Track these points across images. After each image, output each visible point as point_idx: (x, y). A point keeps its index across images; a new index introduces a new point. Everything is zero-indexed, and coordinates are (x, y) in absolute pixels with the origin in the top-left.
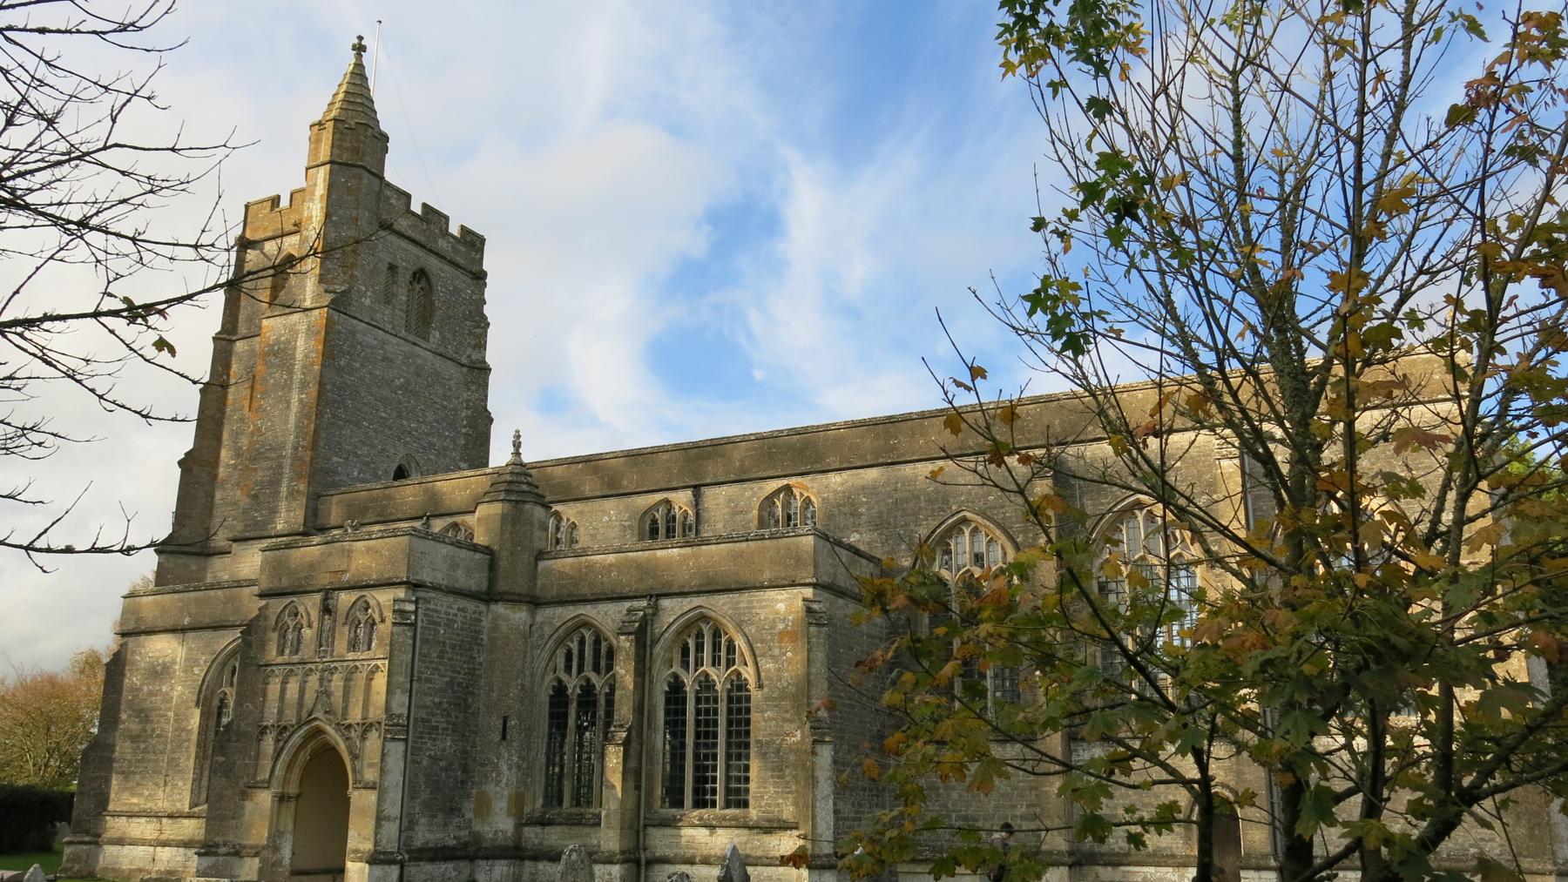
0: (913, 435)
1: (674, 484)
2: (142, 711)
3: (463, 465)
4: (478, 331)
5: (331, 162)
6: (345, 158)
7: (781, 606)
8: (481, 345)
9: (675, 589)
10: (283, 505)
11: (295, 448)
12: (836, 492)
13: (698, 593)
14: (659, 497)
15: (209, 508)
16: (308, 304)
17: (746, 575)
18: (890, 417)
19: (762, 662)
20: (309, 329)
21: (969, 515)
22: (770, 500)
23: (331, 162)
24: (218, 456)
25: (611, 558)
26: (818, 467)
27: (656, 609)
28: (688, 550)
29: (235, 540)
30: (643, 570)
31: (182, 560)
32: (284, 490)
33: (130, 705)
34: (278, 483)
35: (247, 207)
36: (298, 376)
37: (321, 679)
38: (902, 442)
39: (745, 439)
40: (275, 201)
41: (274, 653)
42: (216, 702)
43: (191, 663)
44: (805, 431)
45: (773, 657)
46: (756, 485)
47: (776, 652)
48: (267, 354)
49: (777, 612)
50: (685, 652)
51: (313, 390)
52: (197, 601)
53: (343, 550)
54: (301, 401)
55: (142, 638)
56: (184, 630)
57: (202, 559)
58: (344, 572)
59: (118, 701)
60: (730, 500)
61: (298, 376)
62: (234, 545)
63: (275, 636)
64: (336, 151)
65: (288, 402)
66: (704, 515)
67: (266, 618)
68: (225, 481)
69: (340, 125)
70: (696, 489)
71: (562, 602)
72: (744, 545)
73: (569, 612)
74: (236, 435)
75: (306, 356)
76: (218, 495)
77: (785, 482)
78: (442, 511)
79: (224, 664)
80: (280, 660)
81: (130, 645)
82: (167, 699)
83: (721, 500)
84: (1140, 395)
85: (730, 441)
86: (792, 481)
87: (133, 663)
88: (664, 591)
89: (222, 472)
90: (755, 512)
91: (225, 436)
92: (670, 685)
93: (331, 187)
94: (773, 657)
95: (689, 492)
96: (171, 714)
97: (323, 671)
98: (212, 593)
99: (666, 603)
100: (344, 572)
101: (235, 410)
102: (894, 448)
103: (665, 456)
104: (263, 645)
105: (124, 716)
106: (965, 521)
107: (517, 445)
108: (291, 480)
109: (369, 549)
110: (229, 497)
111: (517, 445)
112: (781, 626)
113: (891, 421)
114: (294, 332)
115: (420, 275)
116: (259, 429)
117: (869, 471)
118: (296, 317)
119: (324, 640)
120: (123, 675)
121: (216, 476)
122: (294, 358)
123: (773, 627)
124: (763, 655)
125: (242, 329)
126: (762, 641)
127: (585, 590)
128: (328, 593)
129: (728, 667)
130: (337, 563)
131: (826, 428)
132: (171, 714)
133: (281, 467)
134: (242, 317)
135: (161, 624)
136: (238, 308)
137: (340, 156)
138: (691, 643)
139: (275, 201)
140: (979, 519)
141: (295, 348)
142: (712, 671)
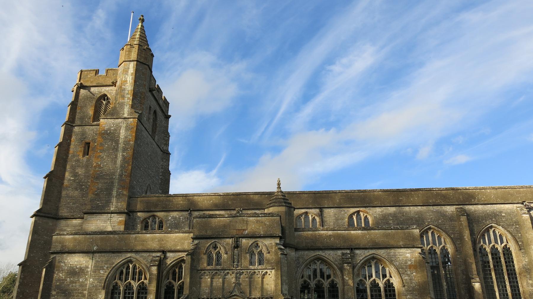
0: (408, 197)
1: (311, 206)
2: (66, 290)
3: (160, 191)
4: (166, 138)
5: (137, 61)
6: (142, 60)
7: (408, 255)
8: (167, 144)
9: (361, 246)
10: (114, 200)
11: (121, 175)
12: (379, 214)
13: (372, 249)
14: (303, 211)
15: (59, 197)
16: (126, 115)
17: (392, 243)
18: (397, 190)
19: (403, 276)
20: (127, 127)
21: (493, 224)
22: (351, 217)
23: (137, 61)
24: (64, 175)
25: (330, 233)
26: (372, 205)
27: (165, 258)
28: (366, 232)
29: (85, 213)
30: (345, 238)
31: (45, 220)
32: (114, 193)
33: (58, 287)
34: (112, 190)
35: (82, 71)
36: (121, 145)
37: (236, 277)
38: (403, 199)
39: (340, 192)
40: (97, 72)
41: (205, 265)
42: (111, 287)
43: (97, 268)
44: (365, 191)
45: (407, 274)
46: (346, 210)
47: (409, 273)
48: (103, 134)
49: (407, 257)
50: (122, 273)
51: (130, 152)
52: (102, 239)
53: (243, 220)
54: (123, 155)
55: (65, 255)
56: (94, 252)
57: (55, 221)
58: (244, 230)
59: (51, 285)
60: (335, 214)
61: (121, 145)
62: (85, 216)
63: (205, 257)
64: (139, 57)
65: (116, 156)
66: (325, 219)
67: (200, 248)
68: (67, 187)
69: (141, 47)
70: (321, 209)
71: (308, 249)
72: (390, 231)
73: (313, 254)
74: (73, 168)
75: (126, 137)
76: (64, 193)
77: (358, 209)
78: (197, 209)
79: (117, 270)
80: (209, 268)
81: (57, 258)
82: (83, 285)
83: (331, 214)
84: (488, 191)
85: (334, 192)
86: (361, 209)
87: (59, 267)
88: (357, 247)
89: (66, 183)
90: (347, 219)
91: (68, 167)
92: (167, 286)
93: (137, 71)
94: (407, 274)
95: (318, 210)
96: (86, 292)
97: (237, 273)
98: (111, 236)
99: (168, 254)
100: (244, 230)
101: (74, 156)
102: (401, 201)
103: (306, 195)
104: (199, 260)
105: (54, 293)
106: (430, 228)
107: (279, 184)
108: (119, 189)
109: (257, 221)
110: (70, 192)
111: (279, 184)
112: (409, 263)
113: (398, 191)
114: (118, 127)
115: (155, 112)
116: (99, 165)
117: (391, 208)
118: (120, 120)
119: (235, 260)
120: (54, 273)
121: (63, 184)
122: (119, 137)
123: (406, 263)
124: (403, 274)
125: (78, 122)
126: (402, 268)
127: (319, 245)
128: (237, 239)
129: (139, 280)
130: (239, 226)
131: (374, 191)
132: (86, 292)
133: (112, 183)
134: (78, 116)
135: (78, 248)
136: (76, 112)
137: (140, 59)
138: (124, 271)
139: (97, 72)
140: (436, 228)
141: (119, 133)
142: (132, 282)
